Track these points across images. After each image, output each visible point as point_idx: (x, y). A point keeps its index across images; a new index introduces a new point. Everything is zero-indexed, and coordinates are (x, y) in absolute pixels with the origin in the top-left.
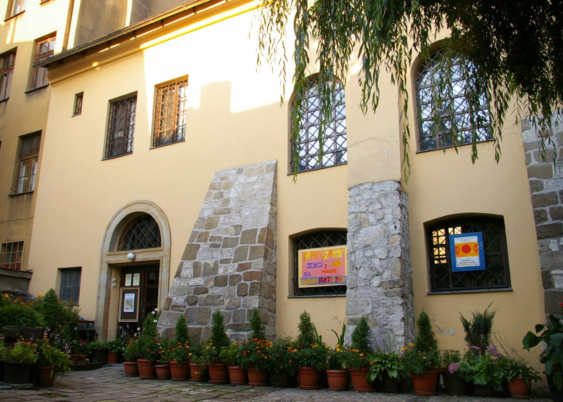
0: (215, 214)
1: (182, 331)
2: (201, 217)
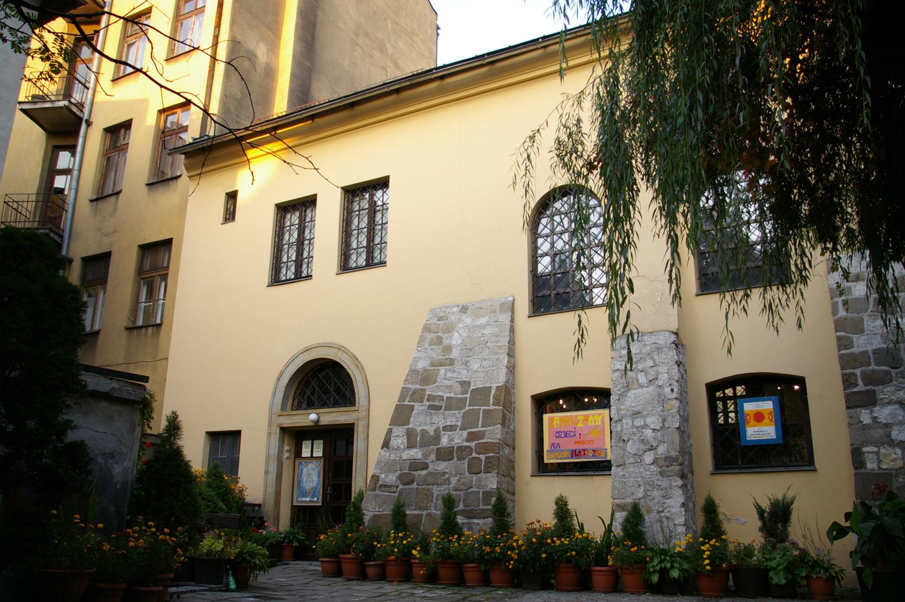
0: (432, 365)
1: (399, 519)
2: (414, 368)
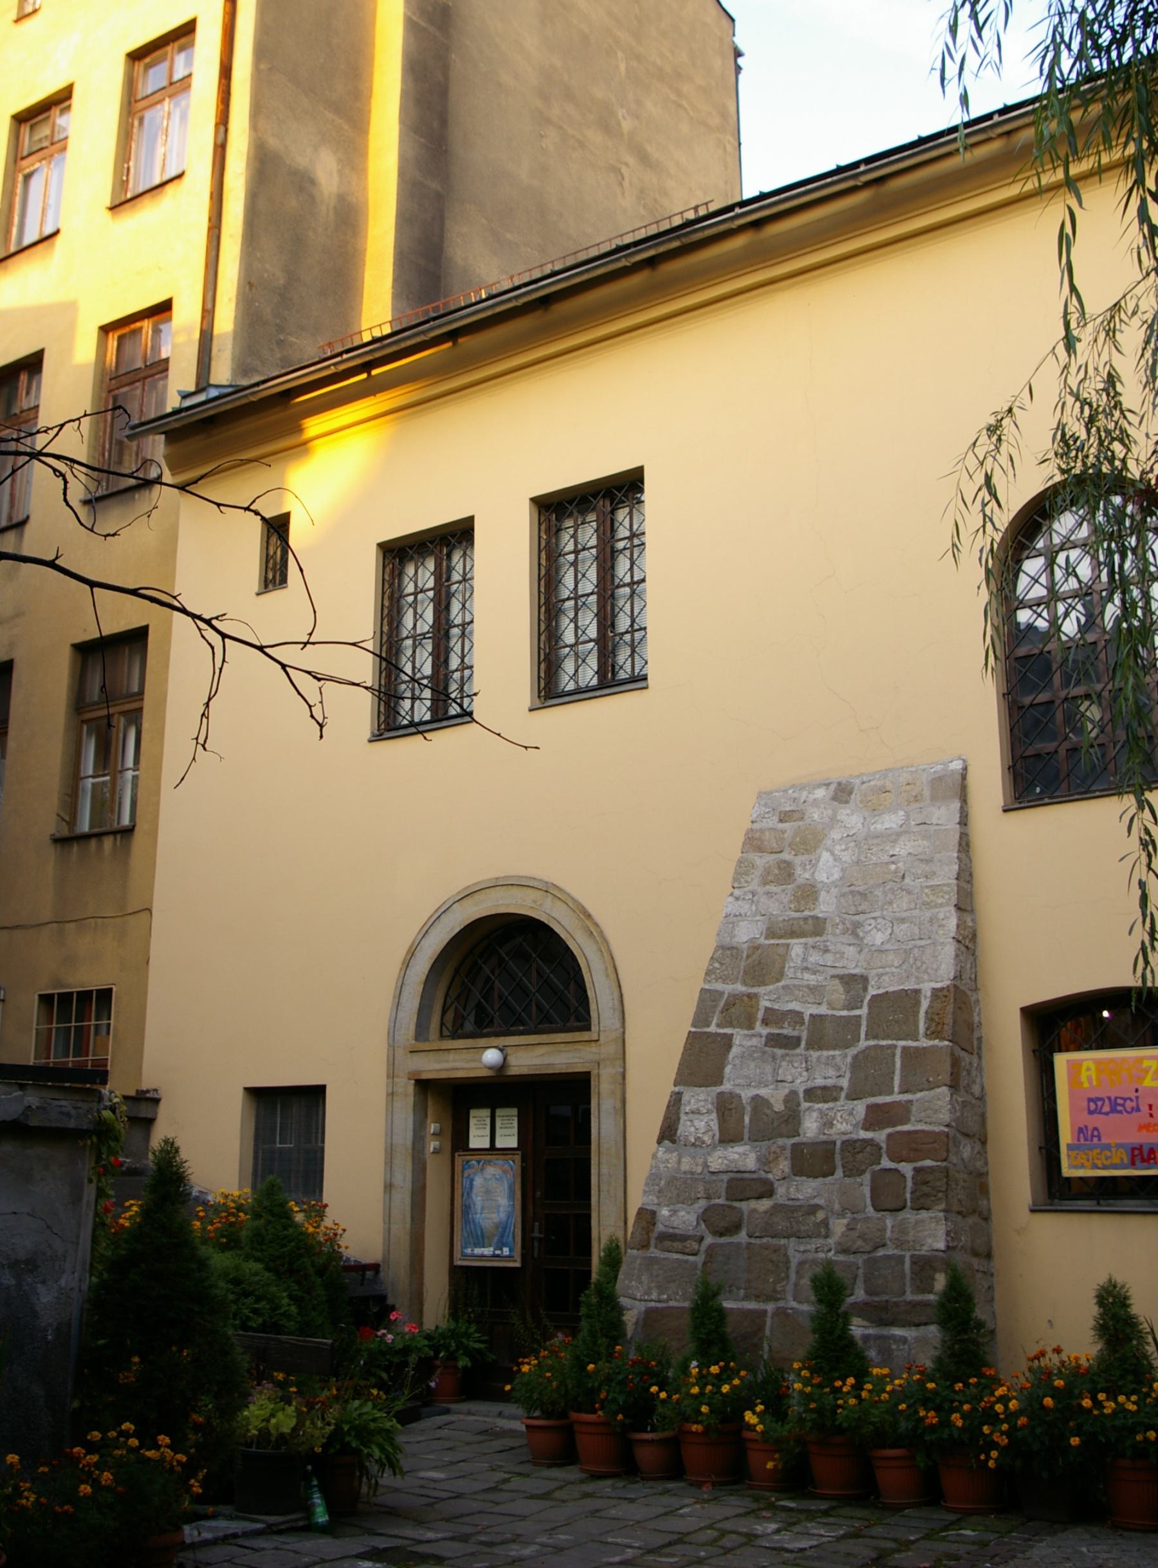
0: (771, 933)
2: (727, 941)
